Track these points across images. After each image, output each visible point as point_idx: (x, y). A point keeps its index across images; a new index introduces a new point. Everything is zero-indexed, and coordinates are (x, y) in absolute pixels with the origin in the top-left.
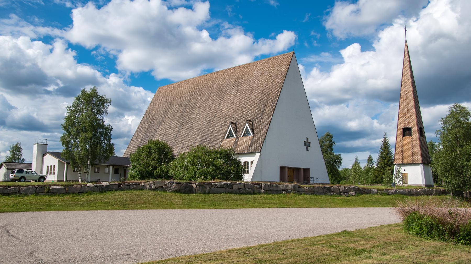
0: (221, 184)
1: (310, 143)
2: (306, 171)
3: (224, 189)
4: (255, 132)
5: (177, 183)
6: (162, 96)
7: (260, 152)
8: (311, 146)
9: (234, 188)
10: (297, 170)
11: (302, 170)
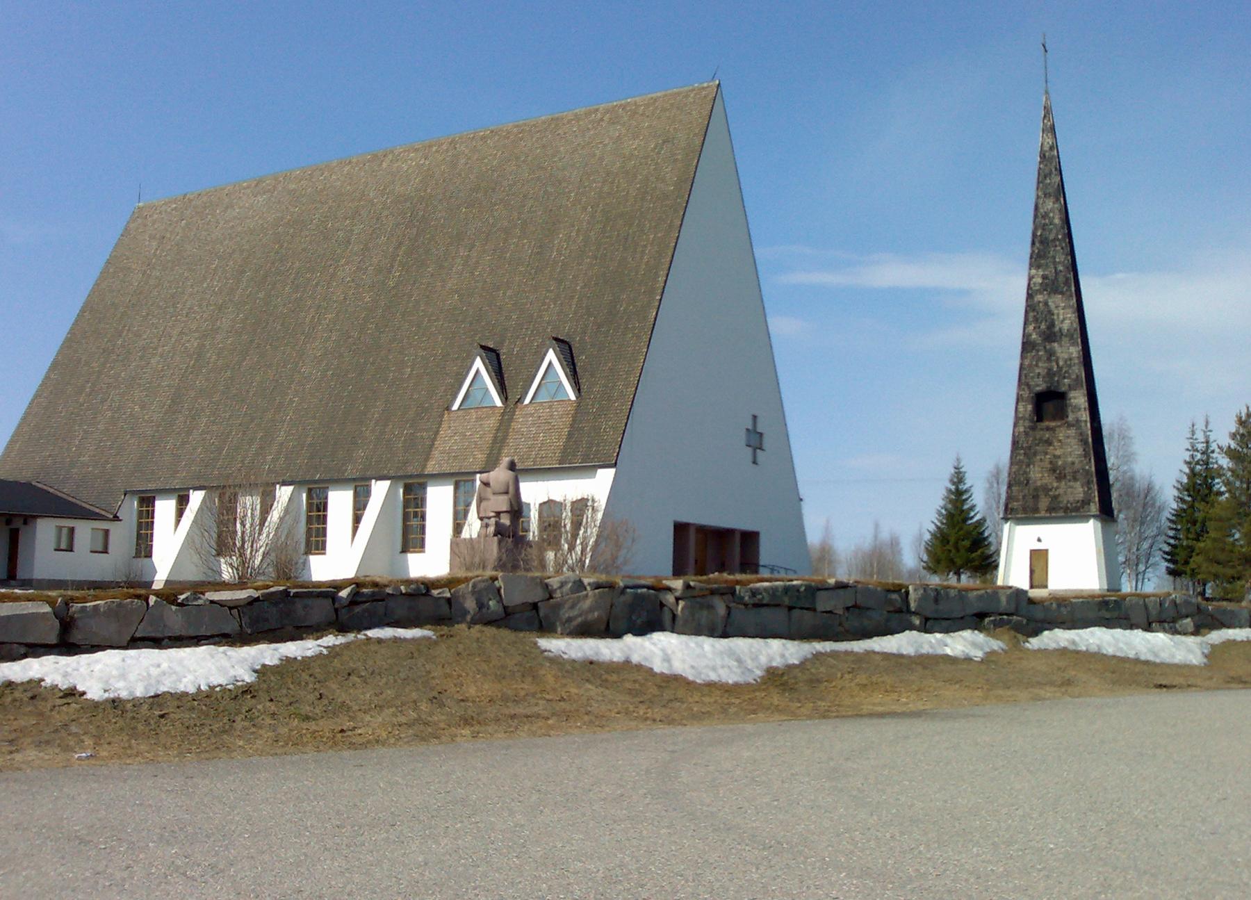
0: (775, 589)
1: (761, 435)
2: (750, 539)
3: (781, 614)
4: (584, 388)
5: (598, 586)
6: (152, 237)
7: (615, 465)
8: (765, 446)
9: (821, 606)
10: (722, 535)
11: (738, 538)
